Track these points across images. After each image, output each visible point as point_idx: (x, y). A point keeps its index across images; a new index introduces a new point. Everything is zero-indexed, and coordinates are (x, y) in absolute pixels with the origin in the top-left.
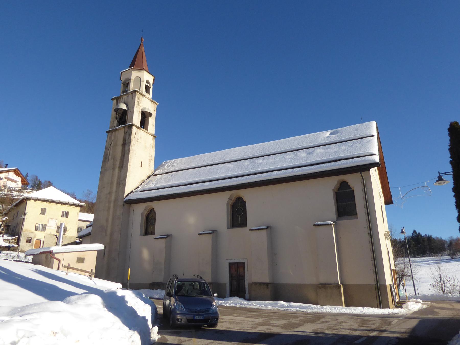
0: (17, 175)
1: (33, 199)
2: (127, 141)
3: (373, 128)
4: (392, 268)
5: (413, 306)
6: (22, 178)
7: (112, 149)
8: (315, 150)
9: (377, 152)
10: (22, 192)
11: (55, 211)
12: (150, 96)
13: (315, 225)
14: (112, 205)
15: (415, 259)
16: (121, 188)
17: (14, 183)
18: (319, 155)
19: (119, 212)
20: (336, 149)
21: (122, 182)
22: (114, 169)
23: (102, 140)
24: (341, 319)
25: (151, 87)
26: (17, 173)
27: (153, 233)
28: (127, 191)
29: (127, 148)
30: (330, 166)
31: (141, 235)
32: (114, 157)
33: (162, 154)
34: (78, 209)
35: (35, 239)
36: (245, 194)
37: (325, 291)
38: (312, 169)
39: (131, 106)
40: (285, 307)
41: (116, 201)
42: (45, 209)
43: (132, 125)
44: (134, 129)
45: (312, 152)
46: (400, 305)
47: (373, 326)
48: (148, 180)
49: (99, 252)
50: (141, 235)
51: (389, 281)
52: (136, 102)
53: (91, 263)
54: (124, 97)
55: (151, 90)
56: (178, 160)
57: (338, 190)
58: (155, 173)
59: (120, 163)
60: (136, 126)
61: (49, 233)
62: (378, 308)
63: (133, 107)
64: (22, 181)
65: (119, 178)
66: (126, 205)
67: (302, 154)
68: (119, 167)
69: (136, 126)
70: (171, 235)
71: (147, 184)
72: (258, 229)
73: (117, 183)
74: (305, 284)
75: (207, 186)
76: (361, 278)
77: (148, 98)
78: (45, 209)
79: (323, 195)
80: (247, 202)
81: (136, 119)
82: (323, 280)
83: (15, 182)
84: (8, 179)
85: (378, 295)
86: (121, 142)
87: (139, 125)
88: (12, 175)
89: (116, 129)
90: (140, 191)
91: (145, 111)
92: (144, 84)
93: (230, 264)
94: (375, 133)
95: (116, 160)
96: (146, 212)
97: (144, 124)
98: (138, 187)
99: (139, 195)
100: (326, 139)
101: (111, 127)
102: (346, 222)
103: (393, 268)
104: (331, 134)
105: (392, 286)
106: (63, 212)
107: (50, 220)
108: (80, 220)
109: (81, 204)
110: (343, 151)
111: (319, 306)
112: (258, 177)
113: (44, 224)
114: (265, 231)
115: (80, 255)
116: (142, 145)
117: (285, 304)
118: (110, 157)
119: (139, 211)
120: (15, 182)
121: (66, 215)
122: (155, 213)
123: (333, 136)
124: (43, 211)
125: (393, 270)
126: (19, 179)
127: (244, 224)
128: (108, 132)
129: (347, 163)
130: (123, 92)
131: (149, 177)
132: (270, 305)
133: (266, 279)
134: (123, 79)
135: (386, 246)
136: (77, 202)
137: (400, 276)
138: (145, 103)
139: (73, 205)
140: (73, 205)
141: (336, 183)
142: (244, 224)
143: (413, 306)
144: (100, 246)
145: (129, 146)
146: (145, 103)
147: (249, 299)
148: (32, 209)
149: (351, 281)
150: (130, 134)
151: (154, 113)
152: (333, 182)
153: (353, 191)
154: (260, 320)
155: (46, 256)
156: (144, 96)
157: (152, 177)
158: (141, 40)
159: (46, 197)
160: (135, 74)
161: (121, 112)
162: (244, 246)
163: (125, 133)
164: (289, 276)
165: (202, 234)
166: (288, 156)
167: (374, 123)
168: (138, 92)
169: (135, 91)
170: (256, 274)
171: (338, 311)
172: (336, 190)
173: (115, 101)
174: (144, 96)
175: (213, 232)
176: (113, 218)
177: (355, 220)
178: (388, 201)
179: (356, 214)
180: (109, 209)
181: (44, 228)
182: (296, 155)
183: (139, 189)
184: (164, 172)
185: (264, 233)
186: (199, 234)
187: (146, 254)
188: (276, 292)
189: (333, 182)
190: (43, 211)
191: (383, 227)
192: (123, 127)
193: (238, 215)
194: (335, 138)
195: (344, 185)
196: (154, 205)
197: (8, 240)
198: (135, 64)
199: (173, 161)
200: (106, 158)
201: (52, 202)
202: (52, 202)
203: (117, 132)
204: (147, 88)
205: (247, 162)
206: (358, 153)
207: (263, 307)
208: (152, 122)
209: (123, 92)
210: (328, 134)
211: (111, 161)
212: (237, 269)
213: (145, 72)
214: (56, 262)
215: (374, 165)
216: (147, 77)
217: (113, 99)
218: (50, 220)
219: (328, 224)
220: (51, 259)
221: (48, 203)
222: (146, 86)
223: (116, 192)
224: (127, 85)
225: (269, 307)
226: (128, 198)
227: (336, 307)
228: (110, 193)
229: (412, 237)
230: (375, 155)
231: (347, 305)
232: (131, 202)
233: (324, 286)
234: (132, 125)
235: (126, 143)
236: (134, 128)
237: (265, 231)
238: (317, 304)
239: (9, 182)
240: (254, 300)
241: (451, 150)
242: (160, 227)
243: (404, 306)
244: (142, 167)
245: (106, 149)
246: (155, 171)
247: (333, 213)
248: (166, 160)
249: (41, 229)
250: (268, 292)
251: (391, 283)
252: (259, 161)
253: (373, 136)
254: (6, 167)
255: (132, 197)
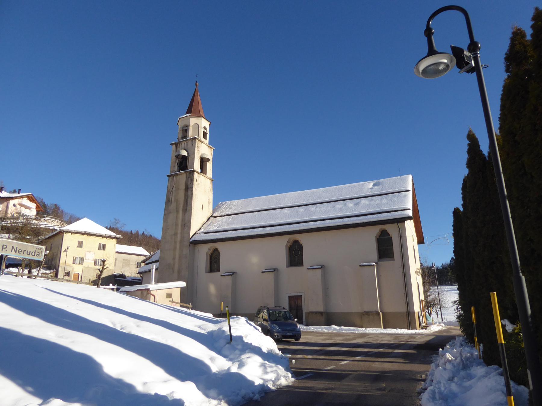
0: (31, 201)
1: (69, 232)
2: (189, 186)
3: (408, 181)
4: (421, 299)
5: (434, 328)
6: (37, 205)
7: (174, 192)
8: (360, 201)
9: (410, 206)
10: (40, 220)
11: (92, 243)
12: (207, 142)
13: (360, 266)
14: (178, 246)
15: (452, 287)
16: (186, 230)
17: (27, 210)
18: (365, 206)
19: (186, 251)
20: (378, 202)
21: (187, 224)
22: (177, 211)
23: (164, 184)
24: (380, 336)
25: (208, 133)
26: (31, 198)
27: (218, 270)
28: (192, 233)
29: (189, 193)
30: (374, 218)
31: (206, 273)
32: (177, 201)
33: (220, 195)
34: (115, 241)
35: (73, 273)
36: (302, 239)
37: (368, 317)
38: (359, 220)
39: (191, 153)
40: (337, 330)
41: (181, 241)
42: (82, 242)
43: (194, 171)
44: (196, 175)
45: (358, 203)
46: (426, 327)
47: (403, 339)
48: (209, 222)
49: (182, 288)
50: (206, 273)
51: (417, 308)
52: (196, 149)
53: (177, 296)
54: (183, 143)
55: (208, 135)
56: (234, 202)
57: (380, 236)
58: (214, 215)
59: (183, 206)
60: (197, 172)
61: (86, 266)
62: (408, 329)
63: (194, 154)
64: (36, 208)
65: (183, 220)
66: (191, 245)
67: (350, 204)
68: (183, 210)
69: (197, 172)
70: (236, 273)
71: (209, 226)
72: (314, 269)
73: (182, 225)
74: (352, 313)
75: (268, 230)
76: (395, 306)
77: (206, 144)
78: (82, 242)
79: (368, 240)
80: (303, 245)
81: (197, 166)
82: (366, 309)
83: (29, 208)
84: (22, 205)
85: (409, 320)
86: (183, 187)
87: (199, 170)
88: (25, 201)
89: (178, 174)
90: (205, 233)
91: (204, 157)
92: (202, 130)
93: (289, 297)
94: (410, 188)
95: (179, 203)
96: (210, 252)
97: (203, 169)
98: (200, 229)
99: (204, 236)
100: (370, 190)
101: (171, 172)
102: (385, 263)
103: (422, 298)
104: (374, 185)
105: (420, 313)
106: (100, 244)
107: (87, 253)
108: (117, 252)
109: (118, 236)
110: (384, 204)
111: (363, 329)
112: (314, 225)
113: (81, 257)
114: (319, 270)
115: (169, 291)
116: (203, 188)
117: (338, 328)
118: (173, 200)
119: (204, 251)
120: (29, 208)
121: (103, 247)
122: (219, 253)
123: (376, 187)
124: (80, 244)
125: (422, 300)
126: (33, 206)
127: (301, 264)
128: (169, 176)
129: (387, 216)
130: (183, 138)
131: (209, 219)
132: (325, 328)
133: (321, 309)
134: (180, 125)
135: (416, 280)
136: (113, 234)
137: (428, 305)
138: (204, 149)
139: (110, 237)
140: (110, 237)
141: (378, 231)
142: (301, 264)
143: (435, 328)
144: (183, 284)
145: (192, 191)
146: (204, 149)
147: (307, 325)
148: (68, 241)
149: (387, 309)
150: (192, 180)
151: (211, 158)
152: (376, 230)
153: (391, 238)
154: (325, 338)
155: (142, 293)
156: (202, 142)
157: (211, 218)
158: (196, 85)
159: (83, 230)
160: (193, 121)
161: (181, 157)
162: (296, 281)
163: (187, 178)
164: (339, 306)
165: (265, 272)
166: (339, 205)
167: (410, 177)
168: (197, 139)
169: (195, 138)
170: (312, 304)
171: (378, 332)
172: (378, 237)
173: (174, 146)
174: (202, 142)
175: (275, 270)
176: (180, 257)
177: (391, 262)
178: (421, 241)
179: (393, 257)
180: (175, 249)
181: (82, 261)
182: (345, 205)
183: (202, 230)
184: (223, 214)
185: (319, 271)
186: (263, 272)
187: (212, 289)
188: (329, 319)
189: (376, 230)
190: (80, 244)
191: (414, 266)
192: (185, 172)
193: (295, 256)
194: (377, 190)
195: (384, 233)
196: (219, 246)
197: (46, 273)
198: (191, 110)
199: (228, 202)
200: (168, 201)
201: (89, 234)
202: (89, 234)
203: (178, 176)
204: (205, 134)
205: (301, 209)
206: (396, 207)
207: (320, 330)
208: (209, 166)
209: (183, 138)
210: (371, 185)
211: (174, 205)
212: (296, 302)
213: (203, 118)
214: (152, 297)
215: (409, 218)
216: (204, 123)
217: (172, 144)
218: (87, 253)
219: (371, 265)
220: (147, 295)
221: (85, 236)
222: (204, 132)
223: (181, 233)
224: (185, 130)
225: (325, 330)
226: (193, 239)
227: (376, 329)
228: (176, 234)
229: (450, 265)
230: (409, 209)
231: (384, 327)
232: (196, 243)
233: (367, 313)
234: (194, 171)
235: (189, 188)
236: (195, 173)
237: (320, 270)
238: (362, 328)
239: (23, 208)
240: (312, 325)
241: (454, 226)
242: (225, 265)
243: (428, 328)
244: (203, 212)
245: (168, 192)
246: (213, 212)
247: (375, 255)
248: (222, 201)
249: (78, 262)
250: (323, 319)
251: (419, 310)
252: (312, 208)
253: (408, 191)
254: (19, 193)
255: (197, 238)
